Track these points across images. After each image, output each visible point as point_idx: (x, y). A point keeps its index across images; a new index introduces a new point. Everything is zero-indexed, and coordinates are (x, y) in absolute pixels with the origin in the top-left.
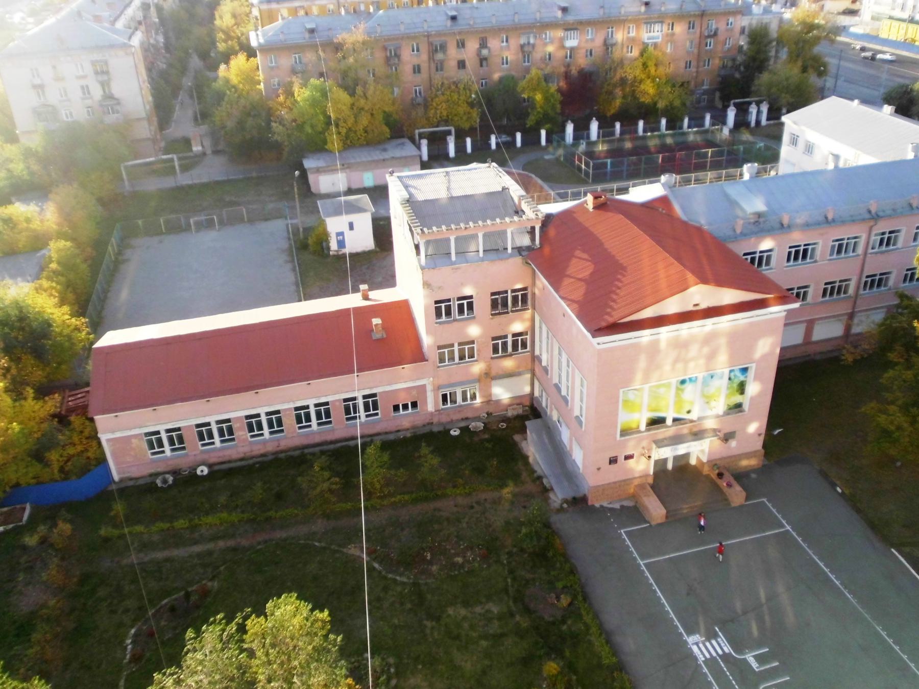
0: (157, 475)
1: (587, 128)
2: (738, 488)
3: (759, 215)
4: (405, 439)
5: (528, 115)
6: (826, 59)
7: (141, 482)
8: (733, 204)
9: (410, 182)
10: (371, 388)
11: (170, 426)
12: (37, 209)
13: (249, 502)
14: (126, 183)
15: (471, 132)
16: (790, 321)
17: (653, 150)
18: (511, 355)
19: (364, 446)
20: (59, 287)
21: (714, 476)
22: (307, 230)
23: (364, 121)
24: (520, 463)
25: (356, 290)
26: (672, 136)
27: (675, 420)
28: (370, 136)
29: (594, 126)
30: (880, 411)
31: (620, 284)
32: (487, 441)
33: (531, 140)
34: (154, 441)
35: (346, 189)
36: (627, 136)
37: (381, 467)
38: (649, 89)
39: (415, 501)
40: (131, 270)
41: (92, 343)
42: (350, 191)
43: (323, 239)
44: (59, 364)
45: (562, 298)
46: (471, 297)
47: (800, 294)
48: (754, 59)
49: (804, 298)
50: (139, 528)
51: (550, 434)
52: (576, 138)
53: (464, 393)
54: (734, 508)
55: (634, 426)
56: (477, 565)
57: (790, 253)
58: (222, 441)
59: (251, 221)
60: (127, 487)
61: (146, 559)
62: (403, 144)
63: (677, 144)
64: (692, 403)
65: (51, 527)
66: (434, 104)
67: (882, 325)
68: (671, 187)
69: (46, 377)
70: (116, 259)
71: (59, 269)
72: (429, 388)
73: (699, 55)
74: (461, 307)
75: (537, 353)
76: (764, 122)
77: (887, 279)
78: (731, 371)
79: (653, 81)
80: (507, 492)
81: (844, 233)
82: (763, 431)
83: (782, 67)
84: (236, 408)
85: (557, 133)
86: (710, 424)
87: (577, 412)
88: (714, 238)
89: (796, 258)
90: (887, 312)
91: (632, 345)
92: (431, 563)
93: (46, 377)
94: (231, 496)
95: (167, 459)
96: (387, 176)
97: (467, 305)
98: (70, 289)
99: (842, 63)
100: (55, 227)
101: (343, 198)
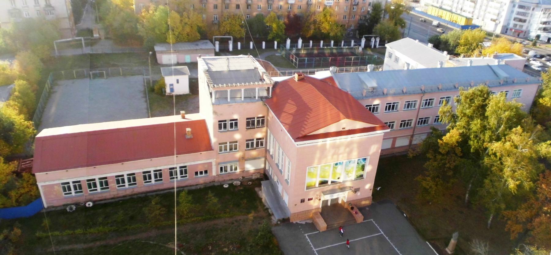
0: (67, 205)
1: (297, 42)
2: (360, 214)
3: (374, 88)
4: (200, 190)
5: (269, 33)
6: (405, 21)
7: (58, 209)
8: (362, 82)
9: (209, 62)
10: (184, 163)
11: (75, 180)
12: (9, 63)
13: (115, 221)
14: (56, 51)
15: (241, 39)
16: (385, 138)
17: (327, 55)
18: (255, 149)
19: (179, 193)
20: (19, 105)
21: (349, 209)
22: (154, 82)
23: (188, 29)
24: (258, 202)
25: (178, 113)
26: (336, 49)
27: (332, 182)
28: (190, 37)
29: (300, 41)
30: (423, 180)
31: (309, 117)
32: (242, 190)
33: (270, 45)
34: (66, 187)
35: (176, 62)
36: (315, 48)
37: (187, 203)
38: (326, 27)
39: (205, 220)
40: (57, 97)
41: (35, 135)
42: (178, 64)
43: (162, 87)
44: (18, 145)
45: (281, 122)
46: (237, 120)
47: (391, 126)
48: (374, 17)
49: (392, 127)
50: (57, 233)
51: (273, 188)
52: (292, 46)
53: (231, 167)
54: (359, 224)
55: (313, 184)
56: (234, 252)
57: (387, 106)
58: (76, 192)
59: (124, 75)
60: (51, 211)
61: (60, 249)
62: (207, 43)
63: (338, 53)
64: (340, 174)
65: (10, 231)
66: (224, 24)
67: (424, 141)
68: (334, 73)
69: (10, 152)
70: (50, 91)
71: (19, 95)
72: (214, 164)
73: (350, 13)
74: (231, 124)
75: (268, 148)
76: (377, 46)
77: (428, 120)
78: (359, 160)
79: (329, 23)
80: (251, 216)
81: (411, 99)
82: (372, 188)
83: (385, 22)
84: (111, 171)
85: (282, 43)
86: (348, 184)
87: (286, 178)
88: (353, 97)
89: (389, 109)
90: (428, 135)
91: (314, 146)
92: (211, 251)
93: (10, 152)
94: (105, 217)
95: (73, 197)
96: (198, 58)
97: (234, 124)
98: (25, 106)
99: (412, 23)
100: (18, 73)
101: (173, 67)
